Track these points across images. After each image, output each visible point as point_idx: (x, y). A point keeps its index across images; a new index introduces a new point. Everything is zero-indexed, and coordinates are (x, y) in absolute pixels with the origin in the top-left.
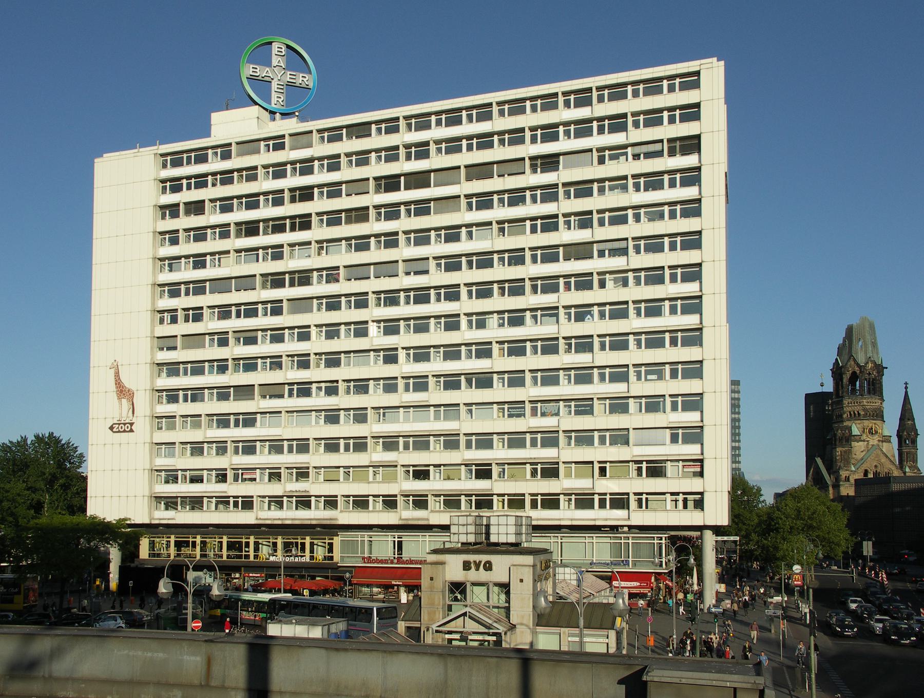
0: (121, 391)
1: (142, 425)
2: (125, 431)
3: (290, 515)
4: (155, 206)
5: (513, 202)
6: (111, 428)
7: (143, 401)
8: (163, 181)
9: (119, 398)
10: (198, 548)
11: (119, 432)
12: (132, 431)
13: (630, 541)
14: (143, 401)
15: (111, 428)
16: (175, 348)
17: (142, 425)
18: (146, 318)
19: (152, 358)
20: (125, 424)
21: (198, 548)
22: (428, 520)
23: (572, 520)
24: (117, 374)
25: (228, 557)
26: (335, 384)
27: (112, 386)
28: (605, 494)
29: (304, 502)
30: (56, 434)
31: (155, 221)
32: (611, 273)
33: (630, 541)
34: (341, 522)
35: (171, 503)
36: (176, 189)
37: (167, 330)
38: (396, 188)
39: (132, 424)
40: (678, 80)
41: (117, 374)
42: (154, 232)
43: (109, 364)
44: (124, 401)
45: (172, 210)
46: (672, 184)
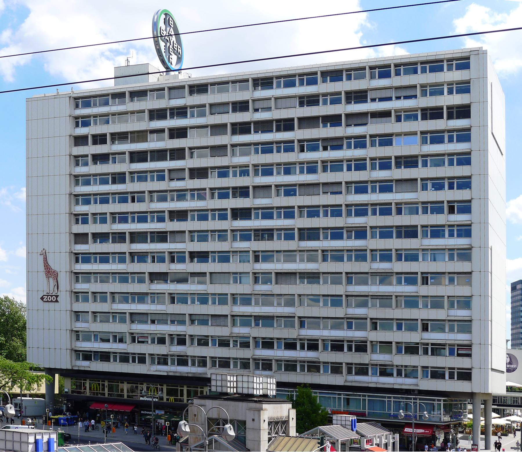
0: (49, 272)
1: (64, 297)
2: (52, 301)
3: (172, 369)
4: (70, 136)
5: (287, 172)
6: (42, 298)
7: (64, 280)
8: (76, 118)
9: (48, 277)
10: (106, 389)
11: (48, 301)
12: (57, 301)
13: (342, 397)
14: (64, 280)
15: (42, 298)
16: (184, 179)
17: (64, 297)
18: (65, 219)
19: (70, 249)
20: (52, 296)
21: (106, 389)
22: (417, 385)
23: (376, 383)
24: (45, 260)
25: (128, 396)
26: (365, 228)
27: (42, 268)
28: (454, 369)
29: (182, 361)
30: (11, 297)
31: (70, 147)
32: (406, 203)
33: (392, 400)
34: (422, 388)
35: (87, 356)
36: (86, 124)
37: (80, 229)
38: (248, 132)
39: (57, 296)
40: (455, 62)
41: (45, 260)
42: (70, 155)
43: (40, 251)
44: (51, 280)
45: (80, 140)
46: (451, 140)
